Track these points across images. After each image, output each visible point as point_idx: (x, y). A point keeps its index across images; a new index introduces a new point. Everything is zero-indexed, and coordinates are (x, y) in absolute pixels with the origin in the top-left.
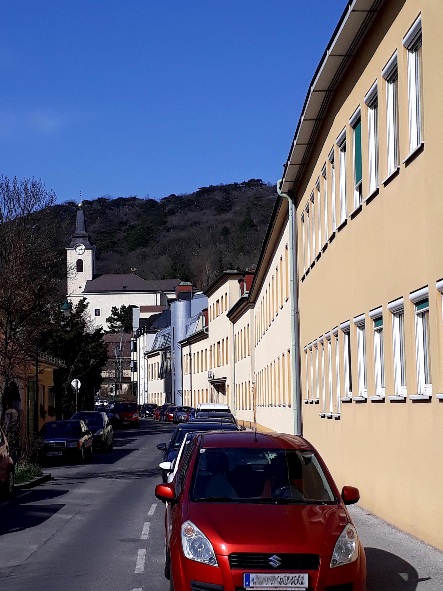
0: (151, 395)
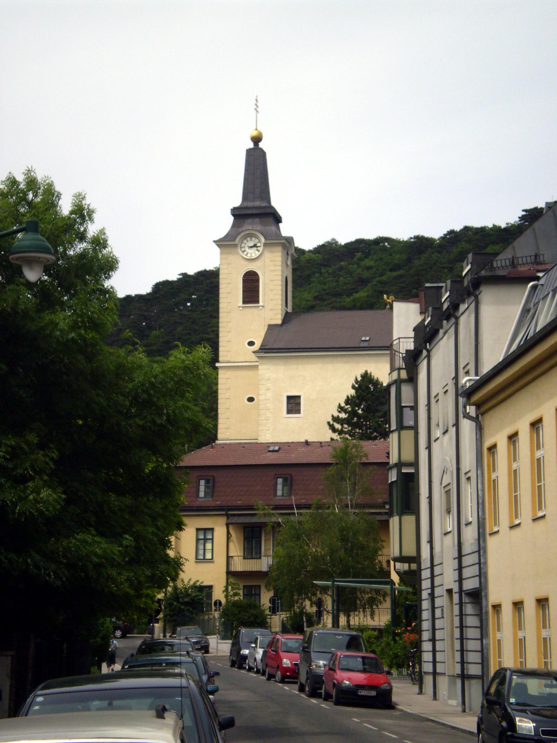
0: (507, 611)
